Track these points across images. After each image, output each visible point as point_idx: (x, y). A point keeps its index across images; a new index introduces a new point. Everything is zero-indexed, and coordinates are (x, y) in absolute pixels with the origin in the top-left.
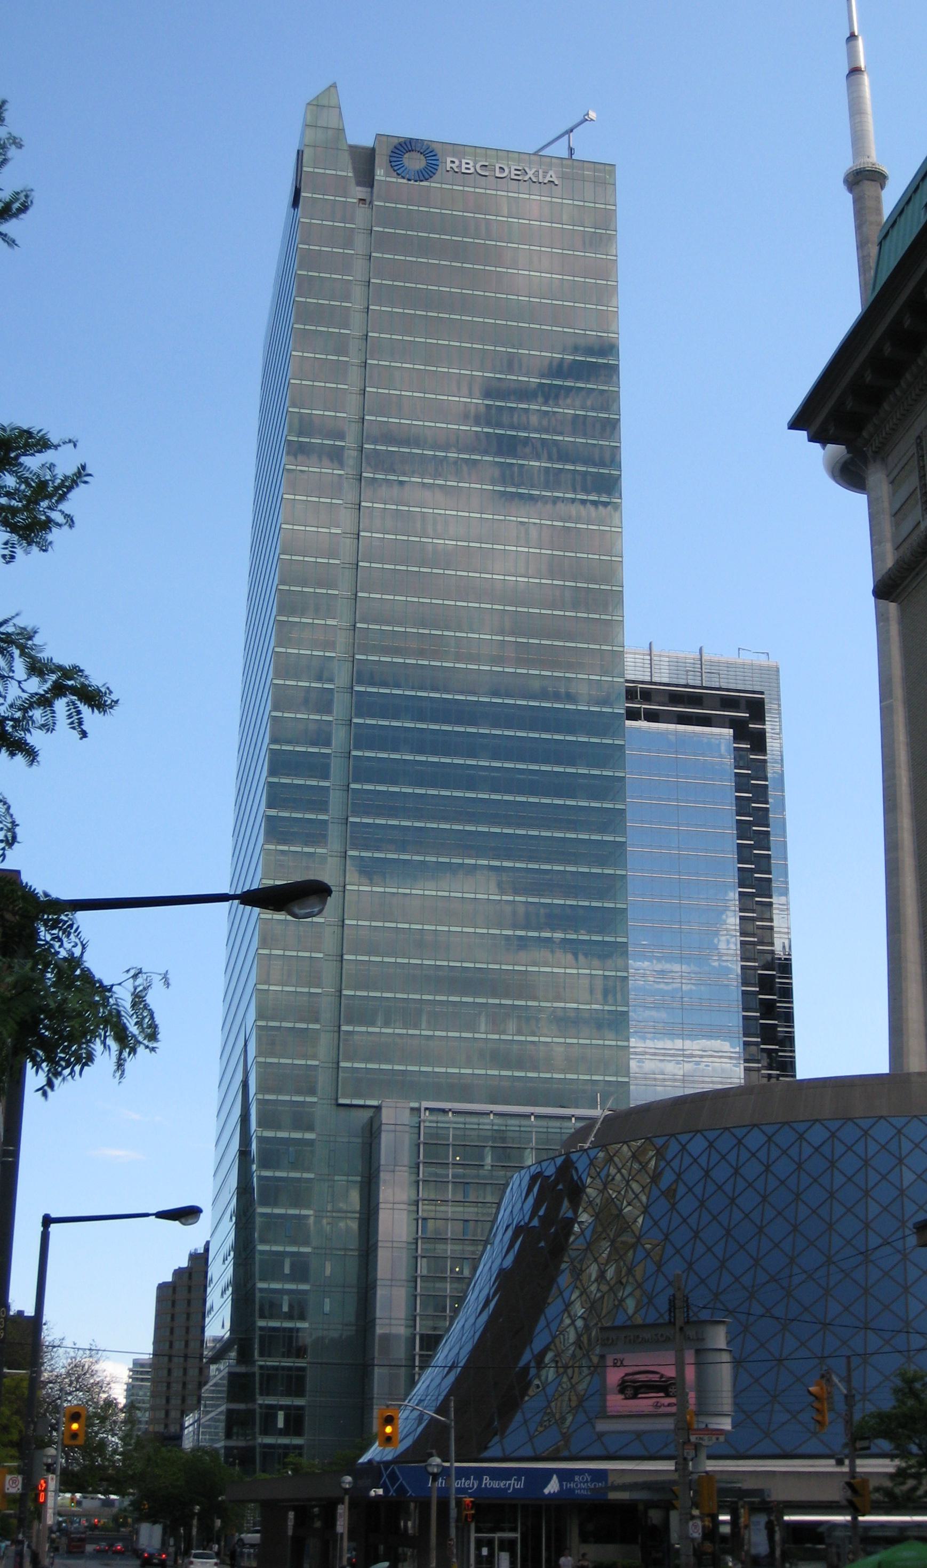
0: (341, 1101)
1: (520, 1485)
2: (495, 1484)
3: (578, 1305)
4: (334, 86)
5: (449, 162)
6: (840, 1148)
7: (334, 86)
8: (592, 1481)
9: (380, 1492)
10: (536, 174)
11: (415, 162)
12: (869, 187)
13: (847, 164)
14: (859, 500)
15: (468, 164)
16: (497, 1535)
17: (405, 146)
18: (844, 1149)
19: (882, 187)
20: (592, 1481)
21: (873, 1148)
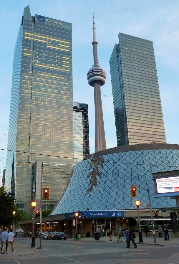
0: (29, 162)
1: (108, 214)
2: (103, 214)
3: (167, 174)
4: (29, 6)
5: (47, 20)
6: (124, 157)
7: (29, 6)
8: (121, 213)
9: (81, 217)
10: (60, 23)
11: (41, 19)
12: (95, 44)
13: (92, 41)
14: (93, 88)
15: (49, 21)
16: (102, 225)
17: (39, 17)
18: (116, 158)
19: (97, 45)
20: (121, 213)
21: (126, 157)
